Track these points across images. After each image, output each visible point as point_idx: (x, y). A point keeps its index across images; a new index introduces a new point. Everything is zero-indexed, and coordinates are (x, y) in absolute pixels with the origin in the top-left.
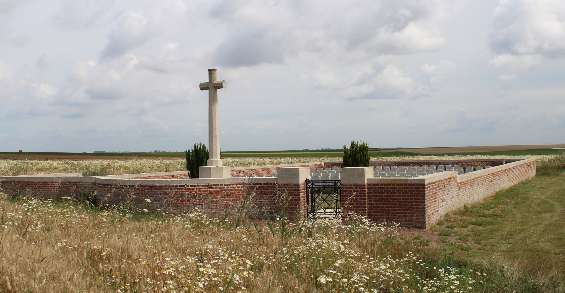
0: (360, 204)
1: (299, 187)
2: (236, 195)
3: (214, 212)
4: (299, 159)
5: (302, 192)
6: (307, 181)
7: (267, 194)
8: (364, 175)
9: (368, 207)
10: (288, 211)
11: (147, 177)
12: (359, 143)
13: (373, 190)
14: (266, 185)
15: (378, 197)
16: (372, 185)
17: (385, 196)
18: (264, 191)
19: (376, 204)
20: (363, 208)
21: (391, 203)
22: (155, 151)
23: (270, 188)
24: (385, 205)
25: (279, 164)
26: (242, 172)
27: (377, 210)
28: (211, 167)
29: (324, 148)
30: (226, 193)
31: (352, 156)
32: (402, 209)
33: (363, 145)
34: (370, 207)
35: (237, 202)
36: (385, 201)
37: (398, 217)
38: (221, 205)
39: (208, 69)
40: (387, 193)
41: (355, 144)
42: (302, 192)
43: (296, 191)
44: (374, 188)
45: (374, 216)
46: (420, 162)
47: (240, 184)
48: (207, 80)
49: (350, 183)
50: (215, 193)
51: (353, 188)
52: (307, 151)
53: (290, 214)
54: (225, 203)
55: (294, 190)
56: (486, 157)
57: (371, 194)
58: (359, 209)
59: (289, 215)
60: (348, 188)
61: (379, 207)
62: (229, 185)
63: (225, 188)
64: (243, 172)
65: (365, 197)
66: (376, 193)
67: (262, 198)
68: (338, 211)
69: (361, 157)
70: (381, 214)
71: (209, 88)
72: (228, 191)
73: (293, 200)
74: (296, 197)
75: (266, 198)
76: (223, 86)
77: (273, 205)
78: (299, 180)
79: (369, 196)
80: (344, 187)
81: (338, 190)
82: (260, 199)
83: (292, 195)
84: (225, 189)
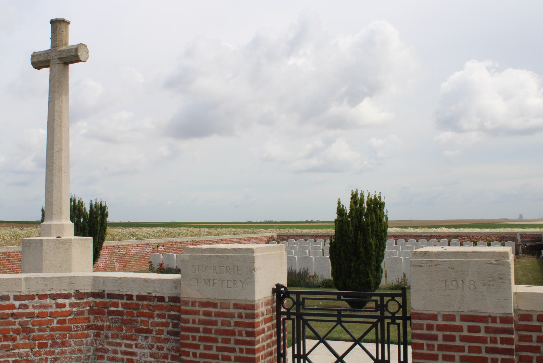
1: (253, 316)
2: (52, 330)
4: (243, 230)
5: (263, 331)
7: (149, 331)
14: (145, 303)
16: (535, 318)
18: (139, 319)
23: (156, 312)
25: (217, 234)
26: (161, 247)
28: (41, 240)
29: (268, 220)
30: (20, 324)
31: (354, 221)
35: (53, 353)
39: (276, 283)
42: (263, 331)
43: (244, 330)
46: (405, 234)
47: (67, 296)
48: (44, 44)
49: (448, 310)
51: (459, 329)
52: (250, 222)
54: (14, 355)
55: (237, 324)
56: (453, 230)
57: (530, 354)
60: (440, 328)
62: (32, 298)
64: (163, 246)
67: (133, 343)
69: (372, 224)
71: (49, 61)
72: (25, 319)
74: (241, 351)
75: (144, 343)
76: (80, 55)
78: (253, 292)
80: (425, 322)
82: (127, 346)
83: (230, 339)
84: (15, 311)
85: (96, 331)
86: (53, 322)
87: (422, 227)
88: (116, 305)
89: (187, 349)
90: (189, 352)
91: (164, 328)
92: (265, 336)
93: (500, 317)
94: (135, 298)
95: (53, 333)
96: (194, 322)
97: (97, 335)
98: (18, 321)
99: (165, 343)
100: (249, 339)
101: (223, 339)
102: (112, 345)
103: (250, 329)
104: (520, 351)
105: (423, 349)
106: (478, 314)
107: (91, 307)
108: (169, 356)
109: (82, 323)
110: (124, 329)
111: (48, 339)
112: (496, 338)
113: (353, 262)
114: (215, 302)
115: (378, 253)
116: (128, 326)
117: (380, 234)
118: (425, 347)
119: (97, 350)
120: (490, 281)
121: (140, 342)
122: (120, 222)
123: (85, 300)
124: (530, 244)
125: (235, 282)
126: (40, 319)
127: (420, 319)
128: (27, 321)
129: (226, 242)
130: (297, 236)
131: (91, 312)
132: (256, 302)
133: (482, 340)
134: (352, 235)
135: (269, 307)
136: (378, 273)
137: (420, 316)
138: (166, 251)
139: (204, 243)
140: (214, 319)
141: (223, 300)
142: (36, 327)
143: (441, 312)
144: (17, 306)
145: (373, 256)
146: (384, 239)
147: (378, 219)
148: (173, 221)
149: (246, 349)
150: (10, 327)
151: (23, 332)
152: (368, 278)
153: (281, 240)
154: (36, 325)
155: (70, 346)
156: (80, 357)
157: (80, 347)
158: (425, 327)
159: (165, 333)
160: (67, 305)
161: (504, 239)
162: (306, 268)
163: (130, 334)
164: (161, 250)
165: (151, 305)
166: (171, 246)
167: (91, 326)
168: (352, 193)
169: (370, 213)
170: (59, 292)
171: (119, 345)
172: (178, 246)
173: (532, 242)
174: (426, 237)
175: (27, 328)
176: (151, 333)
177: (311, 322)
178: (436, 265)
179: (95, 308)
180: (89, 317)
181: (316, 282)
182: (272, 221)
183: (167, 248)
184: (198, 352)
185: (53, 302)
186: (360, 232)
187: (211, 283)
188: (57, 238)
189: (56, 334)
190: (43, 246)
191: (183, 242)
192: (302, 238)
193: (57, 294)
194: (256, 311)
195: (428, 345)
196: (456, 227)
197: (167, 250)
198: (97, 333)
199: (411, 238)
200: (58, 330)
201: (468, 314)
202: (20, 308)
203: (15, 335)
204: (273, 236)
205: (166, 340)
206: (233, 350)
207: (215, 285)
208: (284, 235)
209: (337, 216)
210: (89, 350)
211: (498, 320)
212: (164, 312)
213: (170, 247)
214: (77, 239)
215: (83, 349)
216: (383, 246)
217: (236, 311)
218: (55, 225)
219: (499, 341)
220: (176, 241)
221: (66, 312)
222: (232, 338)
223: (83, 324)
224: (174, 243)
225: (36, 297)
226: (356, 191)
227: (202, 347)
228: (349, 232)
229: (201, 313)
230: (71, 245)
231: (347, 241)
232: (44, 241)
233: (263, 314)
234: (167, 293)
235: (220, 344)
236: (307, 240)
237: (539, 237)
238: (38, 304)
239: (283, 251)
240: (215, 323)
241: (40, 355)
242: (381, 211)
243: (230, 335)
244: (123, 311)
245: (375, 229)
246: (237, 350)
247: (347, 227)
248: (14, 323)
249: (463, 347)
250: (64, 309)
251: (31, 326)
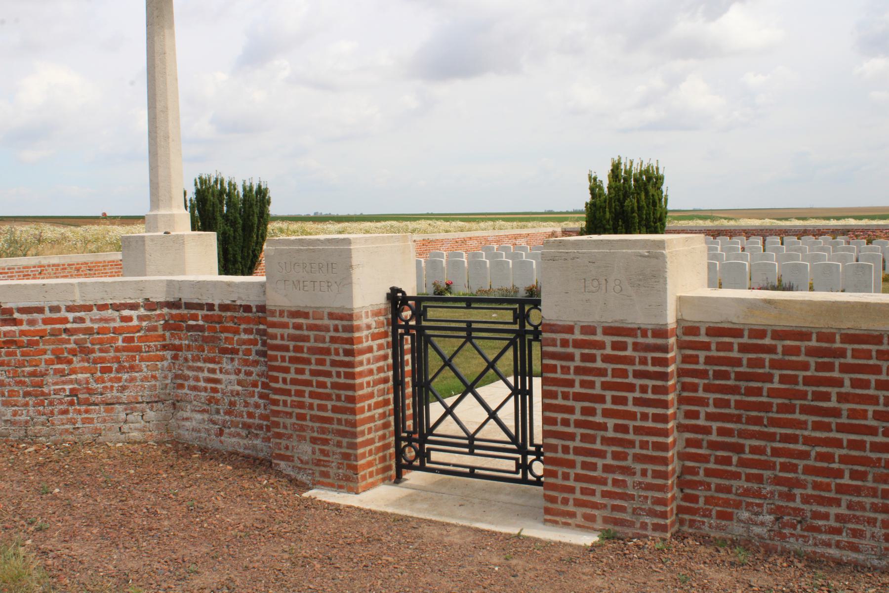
0: (638, 430)
2: (117, 350)
3: (27, 422)
5: (370, 350)
6: (396, 298)
7: (235, 351)
8: (665, 279)
9: (680, 446)
10: (308, 434)
11: (117, 261)
12: (635, 165)
13: (709, 360)
14: (229, 314)
15: (733, 398)
16: (703, 331)
17: (772, 393)
18: (223, 335)
19: (721, 432)
20: (650, 452)
21: (806, 433)
22: (315, 214)
23: (243, 326)
24: (774, 440)
27: (727, 461)
29: (324, 213)
30: (76, 342)
31: (614, 204)
32: (871, 472)
33: (647, 171)
34: (689, 443)
35: (119, 380)
36: (773, 422)
37: (843, 510)
38: (56, 392)
39: (391, 286)
40: (783, 379)
41: (623, 167)
42: (370, 350)
43: (341, 347)
44: (713, 347)
45: (708, 494)
46: (763, 228)
47: (134, 307)
49: (587, 320)
50: (31, 343)
51: (601, 345)
53: (317, 447)
54: (71, 382)
55: (333, 340)
57: (696, 381)
58: (631, 451)
59: (314, 453)
60: (578, 344)
61: (739, 449)
62: (88, 308)
63: (68, 322)
65: (662, 397)
66: (725, 375)
68: (532, 444)
69: (640, 208)
70: (746, 485)
73: (329, 385)
74: (338, 375)
77: (256, 399)
78: (350, 297)
79: (685, 387)
80: (559, 336)
81: (534, 343)
83: (325, 360)
84: (69, 326)
85: (173, 352)
86: (118, 340)
87: (817, 218)
88: (195, 317)
89: (275, 374)
90: (277, 378)
91: (252, 347)
92: (374, 356)
93: (652, 329)
94: (216, 308)
95: (118, 354)
96: (282, 338)
97: (175, 357)
98: (73, 338)
99: (254, 366)
100: (347, 359)
101: (317, 360)
102: (193, 371)
103: (347, 347)
104: (683, 376)
105: (556, 372)
106: (625, 325)
107: (166, 321)
108: (260, 384)
109: (155, 341)
110: (206, 349)
111: (113, 363)
112: (646, 358)
114: (306, 310)
116: (211, 344)
118: (559, 370)
119: (177, 376)
120: (640, 280)
121: (224, 365)
123: (158, 312)
125: (330, 284)
126: (100, 336)
127: (553, 332)
128: (85, 339)
131: (166, 327)
132: (355, 311)
133: (630, 361)
135: (381, 318)
137: (553, 328)
140: (305, 333)
141: (316, 308)
142: (97, 347)
143: (578, 323)
144: (71, 320)
149: (345, 372)
150: (64, 346)
151: (80, 352)
154: (97, 344)
155: (141, 371)
156: (155, 385)
157: (154, 373)
158: (558, 343)
159: (254, 353)
160: (135, 318)
163: (213, 355)
165: (235, 317)
167: (168, 345)
170: (123, 302)
171: (201, 369)
175: (85, 347)
176: (238, 354)
177: (435, 338)
178: (573, 259)
179: (171, 322)
180: (164, 334)
184: (289, 377)
185: (116, 314)
187: (301, 285)
188: (165, 233)
189: (123, 356)
190: (146, 245)
193: (121, 304)
194: (355, 323)
195: (562, 367)
196: (872, 218)
198: (175, 354)
200: (124, 351)
201: (613, 325)
202: (74, 321)
203: (70, 357)
205: (256, 363)
206: (328, 374)
207: (306, 288)
210: (165, 377)
211: (650, 334)
212: (251, 326)
214: (194, 235)
215: (157, 375)
217: (331, 323)
218: (163, 215)
219: (650, 361)
221: (134, 327)
222: (328, 358)
223: (157, 343)
225: (95, 308)
227: (292, 370)
229: (291, 326)
230: (183, 243)
232: (146, 239)
233: (369, 327)
234: (253, 300)
235: (313, 367)
238: (97, 317)
239: (410, 243)
240: (306, 339)
241: (103, 382)
243: (325, 354)
244: (203, 326)
246: (334, 374)
247: (602, 214)
248: (68, 341)
249: (606, 370)
250: (130, 324)
251: (90, 345)
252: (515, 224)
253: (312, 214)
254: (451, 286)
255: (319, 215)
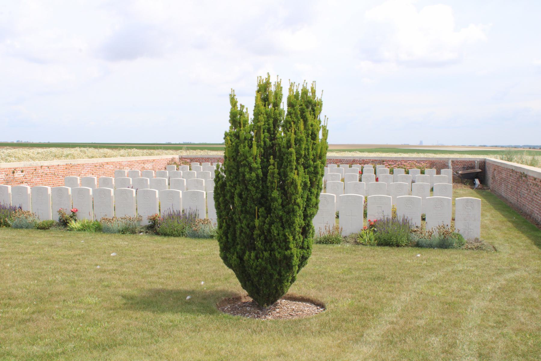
22: (17, 141)
26: (19, 172)
29: (186, 142)
31: (262, 136)
64: (22, 172)
69: (298, 141)
113: (258, 217)
115: (309, 200)
117: (312, 163)
122: (40, 143)
124: (463, 172)
129: (113, 166)
130: (202, 158)
134: (256, 163)
136: (306, 237)
138: (27, 177)
139: (83, 167)
145: (298, 208)
146: (320, 173)
147: (310, 132)
148: (94, 142)
152: (286, 250)
153: (183, 163)
161: (433, 165)
162: (194, 209)
164: (19, 177)
166: (34, 172)
168: (260, 83)
169: (295, 120)
172: (44, 171)
173: (464, 169)
174: (348, 161)
181: (207, 229)
182: (191, 143)
183: (29, 174)
186: (274, 158)
191: (52, 166)
192: (208, 161)
197: (28, 176)
199: (331, 163)
204: (174, 158)
208: (187, 157)
209: (230, 127)
213: (33, 173)
216: (318, 185)
220: (42, 165)
224: (38, 167)
226: (267, 77)
228: (251, 158)
231: (247, 176)
236: (214, 163)
237: (472, 164)
242: (315, 119)
245: (303, 153)
247: (247, 148)
252: (145, 151)
253: (15, 142)
254: (77, 213)
255: (20, 142)
